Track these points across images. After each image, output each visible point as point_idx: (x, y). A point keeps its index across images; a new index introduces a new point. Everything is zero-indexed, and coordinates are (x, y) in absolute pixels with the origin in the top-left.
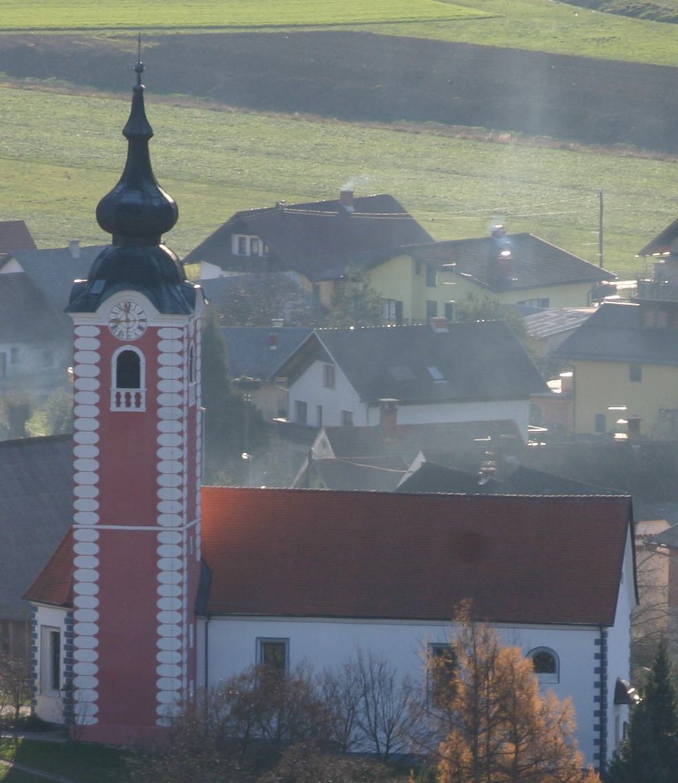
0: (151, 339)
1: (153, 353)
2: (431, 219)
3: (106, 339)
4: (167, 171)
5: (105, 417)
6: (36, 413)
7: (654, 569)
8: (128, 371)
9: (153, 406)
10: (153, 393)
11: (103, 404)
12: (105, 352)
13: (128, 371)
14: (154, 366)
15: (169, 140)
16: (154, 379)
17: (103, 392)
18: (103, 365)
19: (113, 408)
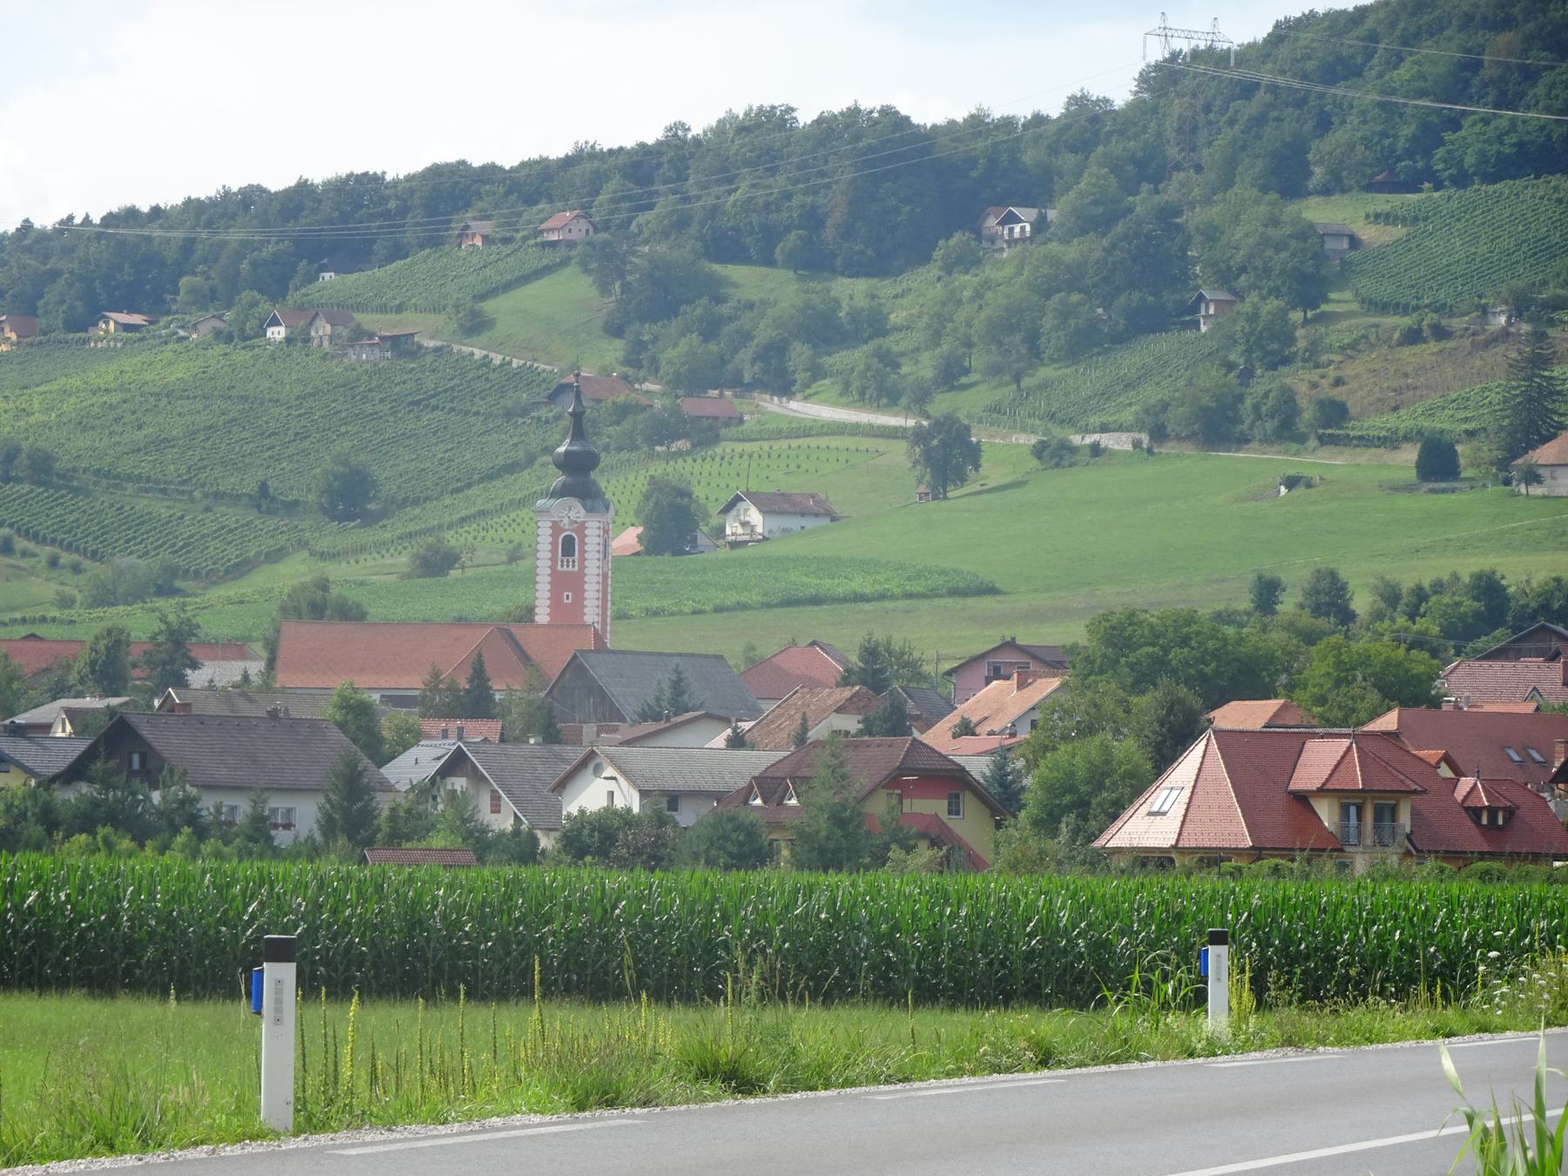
0: (582, 527)
1: (583, 537)
2: (250, 487)
3: (556, 528)
4: (82, 425)
5: (554, 574)
6: (404, 786)
7: (1391, 489)
8: (568, 547)
9: (582, 567)
10: (582, 559)
11: (554, 567)
12: (555, 536)
13: (568, 547)
14: (582, 544)
15: (1510, 892)
16: (583, 551)
17: (553, 559)
18: (554, 544)
19: (559, 568)
